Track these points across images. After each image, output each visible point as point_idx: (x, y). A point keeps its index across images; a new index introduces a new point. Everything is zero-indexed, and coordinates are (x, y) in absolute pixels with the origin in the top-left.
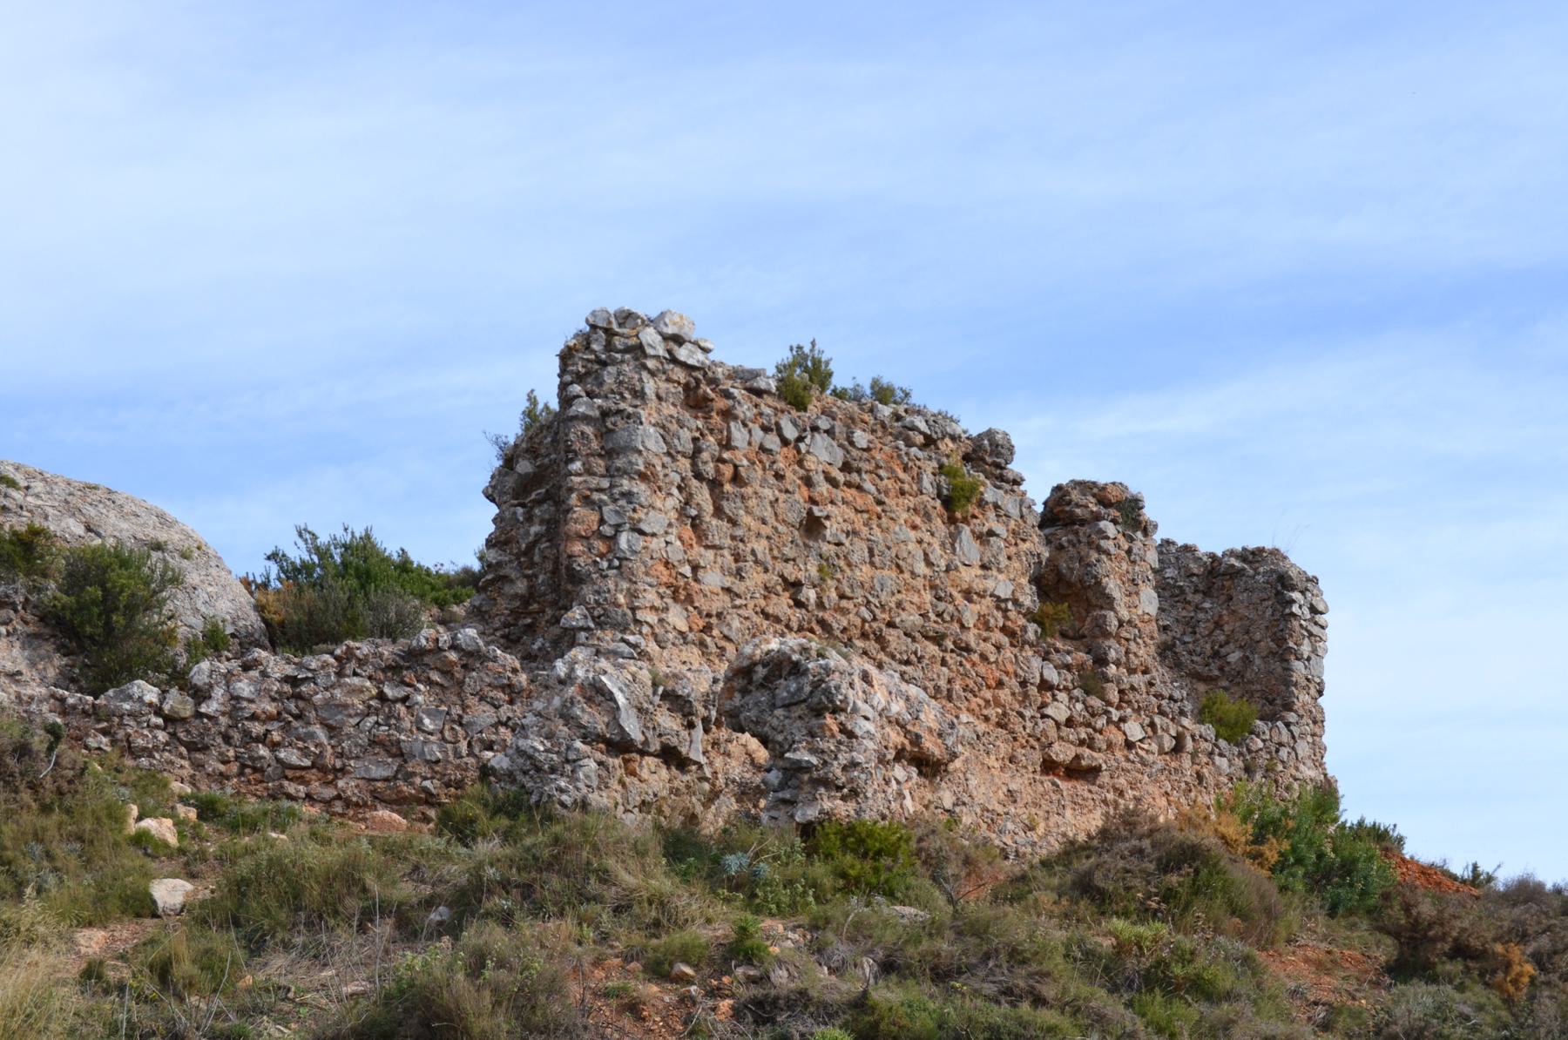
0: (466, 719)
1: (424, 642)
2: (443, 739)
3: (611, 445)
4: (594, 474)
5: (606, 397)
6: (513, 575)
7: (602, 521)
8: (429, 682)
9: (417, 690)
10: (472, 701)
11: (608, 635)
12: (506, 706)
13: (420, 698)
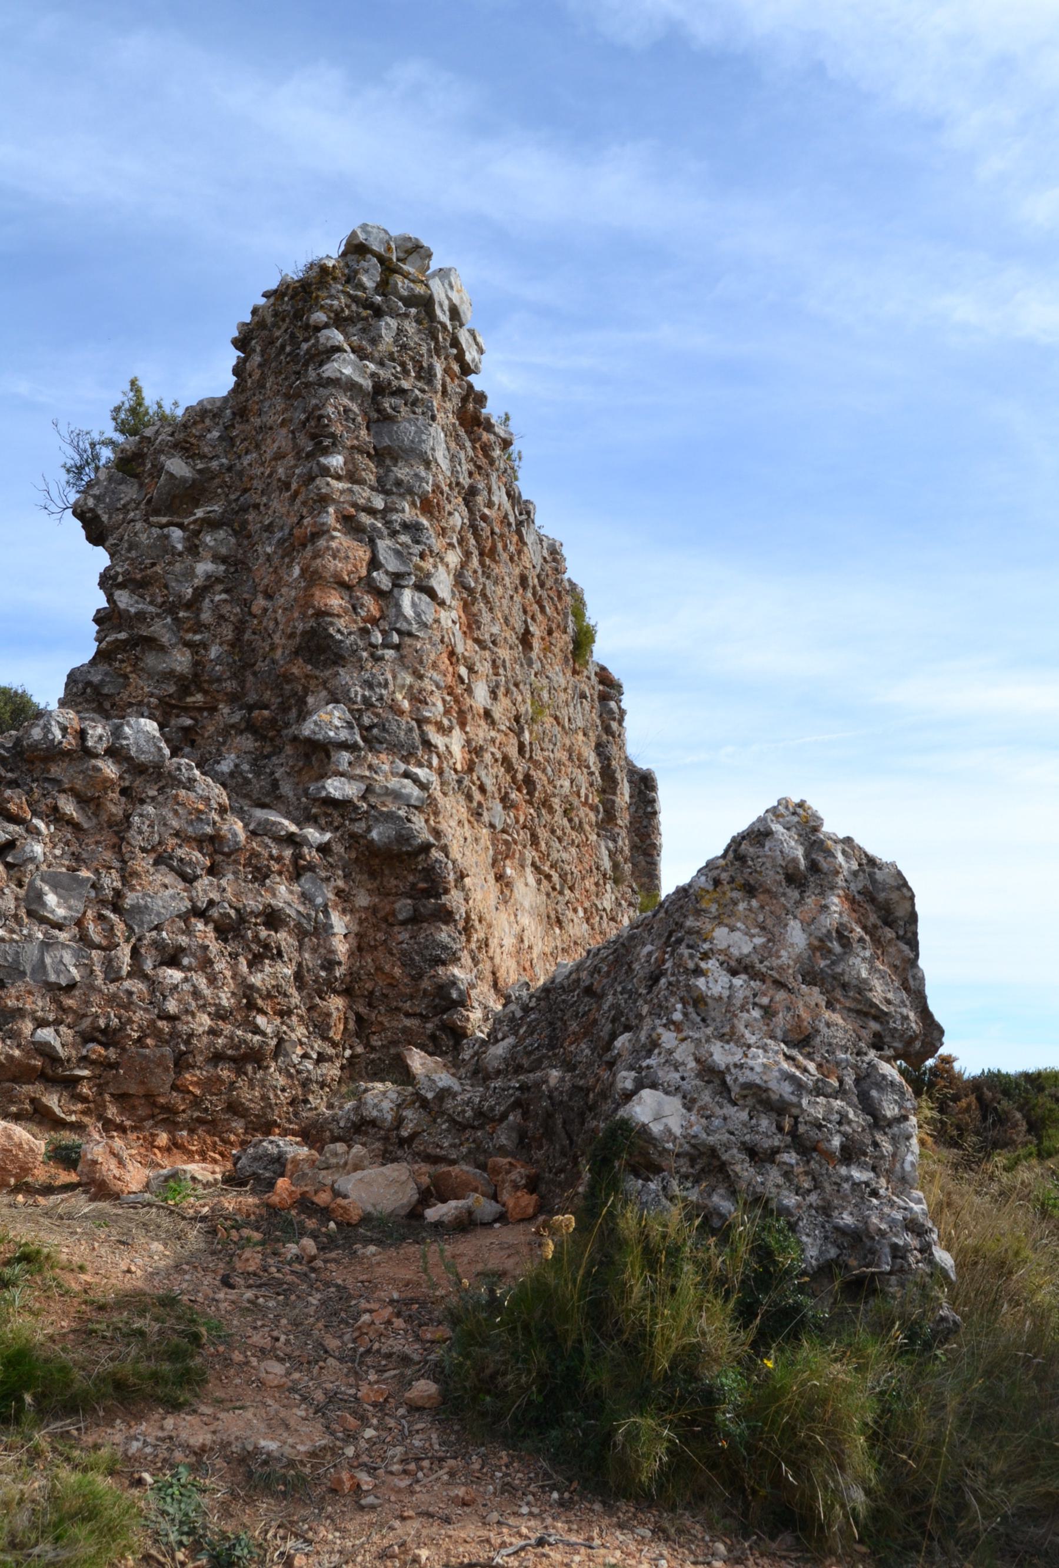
0: (130, 899)
1: (58, 734)
2: (83, 938)
3: (386, 442)
4: (360, 482)
5: (381, 364)
6: (166, 638)
7: (374, 563)
8: (55, 816)
9: (35, 832)
10: (143, 863)
11: (384, 762)
12: (206, 880)
13: (38, 849)
